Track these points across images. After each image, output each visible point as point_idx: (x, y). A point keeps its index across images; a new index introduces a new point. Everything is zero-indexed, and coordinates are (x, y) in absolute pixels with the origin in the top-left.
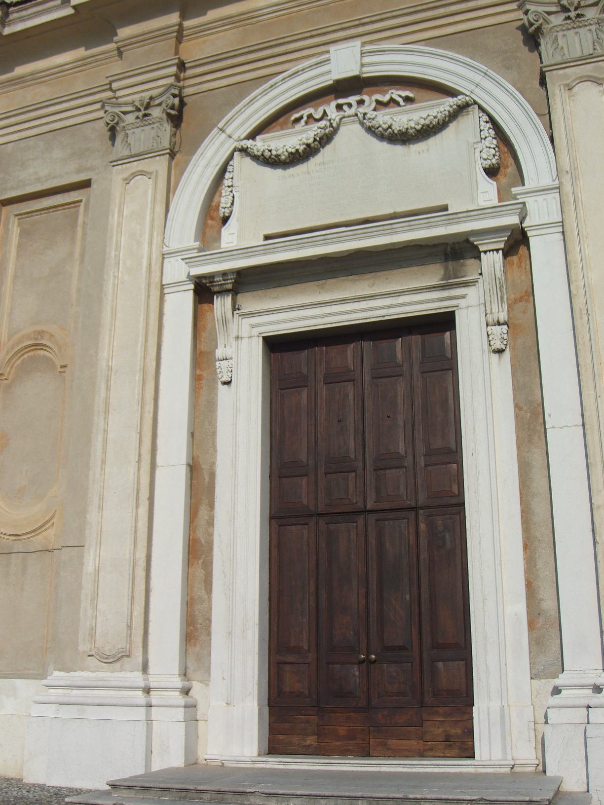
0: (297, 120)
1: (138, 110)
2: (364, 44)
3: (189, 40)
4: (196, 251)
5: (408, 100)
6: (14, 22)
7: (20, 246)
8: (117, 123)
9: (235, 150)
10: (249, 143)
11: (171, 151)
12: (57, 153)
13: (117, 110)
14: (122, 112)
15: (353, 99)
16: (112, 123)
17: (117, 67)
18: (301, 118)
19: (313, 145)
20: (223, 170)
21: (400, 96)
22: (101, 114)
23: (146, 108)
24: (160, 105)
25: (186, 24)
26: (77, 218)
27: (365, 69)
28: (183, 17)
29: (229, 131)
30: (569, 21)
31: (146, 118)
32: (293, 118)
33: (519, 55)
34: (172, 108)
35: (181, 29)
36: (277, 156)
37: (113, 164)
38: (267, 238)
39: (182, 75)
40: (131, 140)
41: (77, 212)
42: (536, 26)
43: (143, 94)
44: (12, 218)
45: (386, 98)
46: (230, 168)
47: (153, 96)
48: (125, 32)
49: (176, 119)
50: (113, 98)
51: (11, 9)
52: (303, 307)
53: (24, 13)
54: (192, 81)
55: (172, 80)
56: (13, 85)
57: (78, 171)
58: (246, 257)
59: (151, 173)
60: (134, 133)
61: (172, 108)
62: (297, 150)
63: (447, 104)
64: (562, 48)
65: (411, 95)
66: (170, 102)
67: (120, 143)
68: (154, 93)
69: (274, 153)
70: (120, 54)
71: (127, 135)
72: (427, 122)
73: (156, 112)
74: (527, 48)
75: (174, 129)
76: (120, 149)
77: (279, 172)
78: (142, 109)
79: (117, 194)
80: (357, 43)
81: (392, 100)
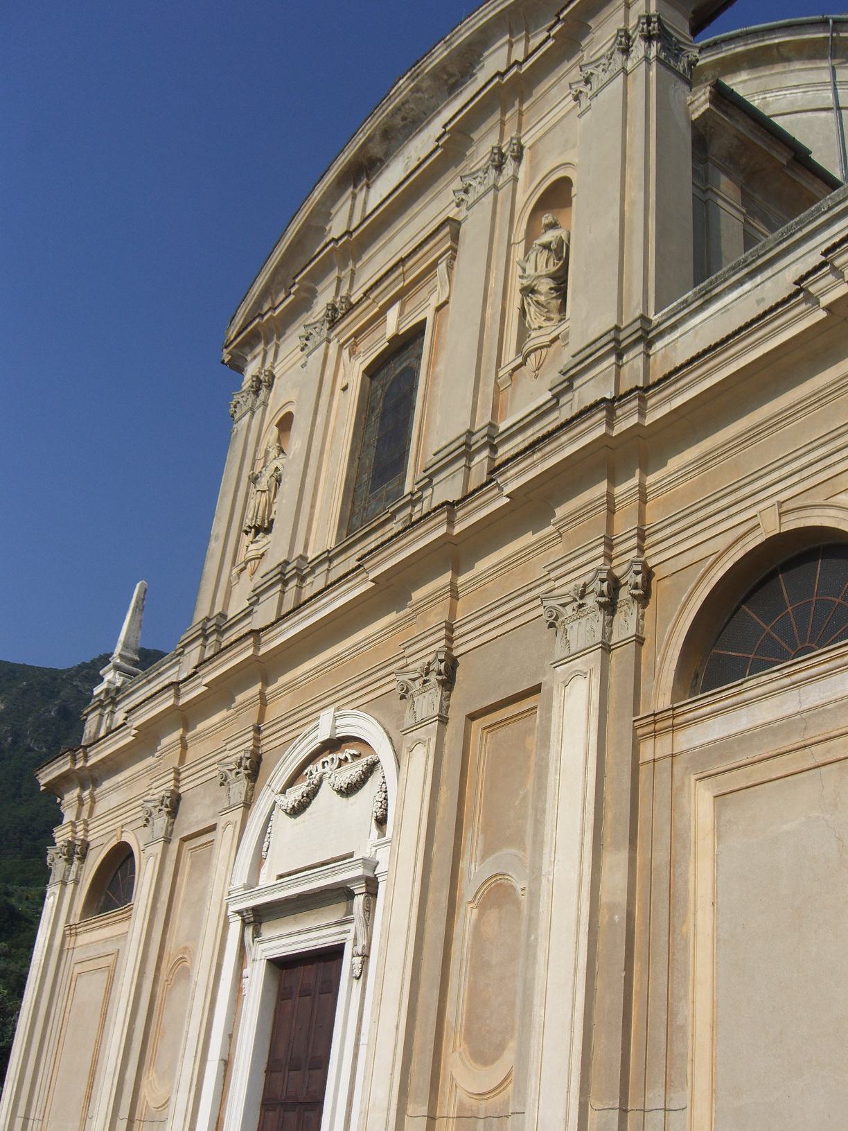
1: (575, 600)
2: (338, 709)
4: (243, 889)
6: (267, 643)
7: (190, 875)
19: (302, 800)
20: (269, 819)
22: (541, 611)
23: (581, 598)
24: (592, 591)
27: (338, 731)
37: (404, 733)
38: (280, 877)
43: (577, 582)
47: (587, 582)
52: (282, 937)
54: (186, 781)
56: (195, 739)
58: (252, 899)
62: (294, 806)
65: (356, 753)
68: (587, 579)
71: (566, 631)
73: (591, 601)
78: (578, 599)
80: (331, 709)
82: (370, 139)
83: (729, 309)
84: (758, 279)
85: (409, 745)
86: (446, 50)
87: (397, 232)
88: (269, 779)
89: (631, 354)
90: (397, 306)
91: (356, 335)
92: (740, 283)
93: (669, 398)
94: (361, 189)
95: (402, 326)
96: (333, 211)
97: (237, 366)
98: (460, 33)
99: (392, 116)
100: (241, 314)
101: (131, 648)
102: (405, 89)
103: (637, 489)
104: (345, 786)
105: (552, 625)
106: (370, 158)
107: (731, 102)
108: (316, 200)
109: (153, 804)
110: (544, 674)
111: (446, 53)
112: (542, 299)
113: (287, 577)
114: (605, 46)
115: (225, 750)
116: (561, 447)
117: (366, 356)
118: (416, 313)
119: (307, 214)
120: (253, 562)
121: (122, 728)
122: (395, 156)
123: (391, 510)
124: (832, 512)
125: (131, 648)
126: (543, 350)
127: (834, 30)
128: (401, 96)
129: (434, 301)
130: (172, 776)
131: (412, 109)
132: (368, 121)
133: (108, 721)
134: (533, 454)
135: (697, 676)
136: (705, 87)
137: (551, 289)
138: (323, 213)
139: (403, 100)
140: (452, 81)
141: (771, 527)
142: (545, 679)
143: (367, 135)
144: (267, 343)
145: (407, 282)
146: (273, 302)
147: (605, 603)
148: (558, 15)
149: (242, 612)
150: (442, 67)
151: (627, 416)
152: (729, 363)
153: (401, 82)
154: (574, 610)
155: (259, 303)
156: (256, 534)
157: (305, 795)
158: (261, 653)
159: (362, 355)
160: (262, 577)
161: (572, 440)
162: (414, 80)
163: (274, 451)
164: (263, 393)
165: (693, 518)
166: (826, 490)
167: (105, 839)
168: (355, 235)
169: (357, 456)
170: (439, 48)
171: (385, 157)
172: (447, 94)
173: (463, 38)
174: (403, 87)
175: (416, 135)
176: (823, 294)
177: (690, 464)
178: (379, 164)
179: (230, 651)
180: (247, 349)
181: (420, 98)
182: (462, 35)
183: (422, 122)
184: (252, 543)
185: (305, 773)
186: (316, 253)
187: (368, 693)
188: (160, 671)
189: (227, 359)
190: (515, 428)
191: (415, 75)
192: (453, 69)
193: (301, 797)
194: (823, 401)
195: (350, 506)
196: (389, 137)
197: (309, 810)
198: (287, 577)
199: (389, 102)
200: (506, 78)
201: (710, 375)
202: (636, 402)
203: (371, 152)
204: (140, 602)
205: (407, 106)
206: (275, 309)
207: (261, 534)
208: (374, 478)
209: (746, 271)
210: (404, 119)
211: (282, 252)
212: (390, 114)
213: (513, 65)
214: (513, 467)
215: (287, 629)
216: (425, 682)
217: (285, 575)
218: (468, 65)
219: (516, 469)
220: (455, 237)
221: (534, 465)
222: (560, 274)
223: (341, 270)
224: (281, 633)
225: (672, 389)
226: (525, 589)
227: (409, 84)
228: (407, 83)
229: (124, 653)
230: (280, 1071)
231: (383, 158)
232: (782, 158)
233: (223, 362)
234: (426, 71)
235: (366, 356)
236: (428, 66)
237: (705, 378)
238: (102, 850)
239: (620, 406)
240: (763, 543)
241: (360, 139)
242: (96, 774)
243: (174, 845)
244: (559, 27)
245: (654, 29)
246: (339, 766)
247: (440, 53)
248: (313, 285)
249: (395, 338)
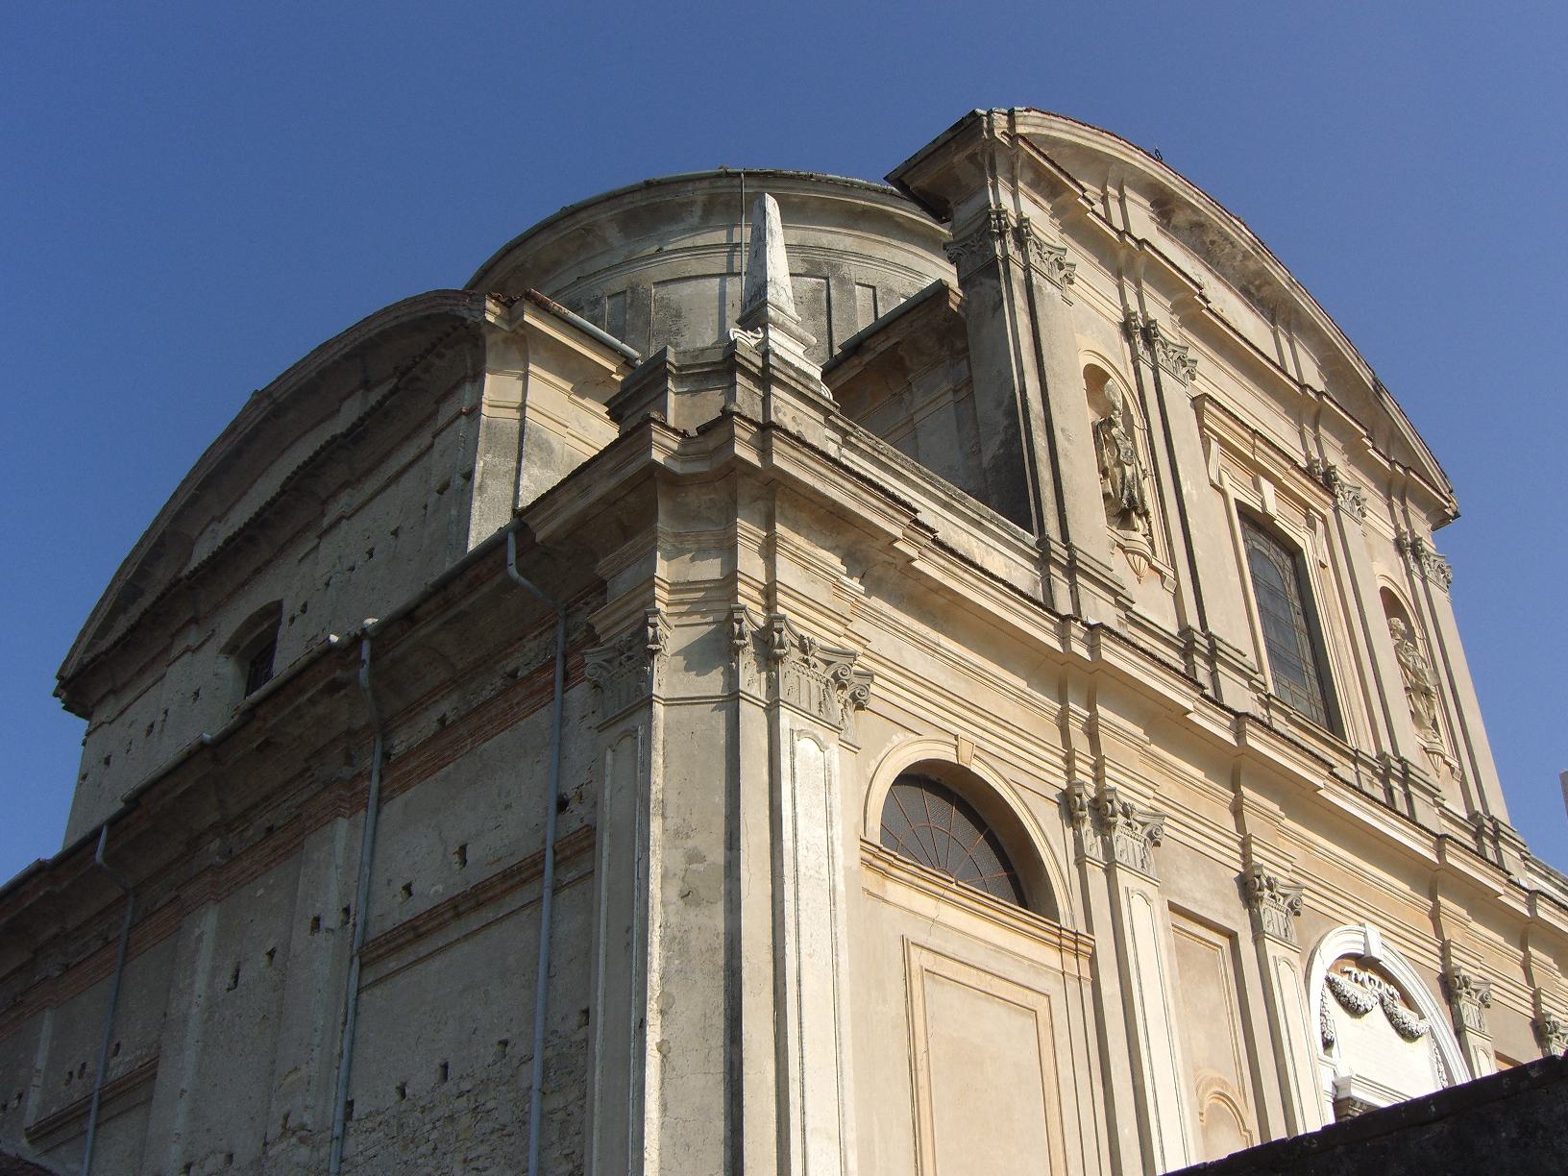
58: (1379, 1097)
106: (1174, 211)
118: (1241, 489)
122: (1182, 247)
140: (1253, 290)
148: (1410, 468)
150: (1269, 280)
162: (1253, 249)
179: (1297, 752)
181: (1235, 258)
186: (1081, 183)
192: (1266, 291)
203: (1181, 212)
210: (1213, 243)
215: (1351, 802)
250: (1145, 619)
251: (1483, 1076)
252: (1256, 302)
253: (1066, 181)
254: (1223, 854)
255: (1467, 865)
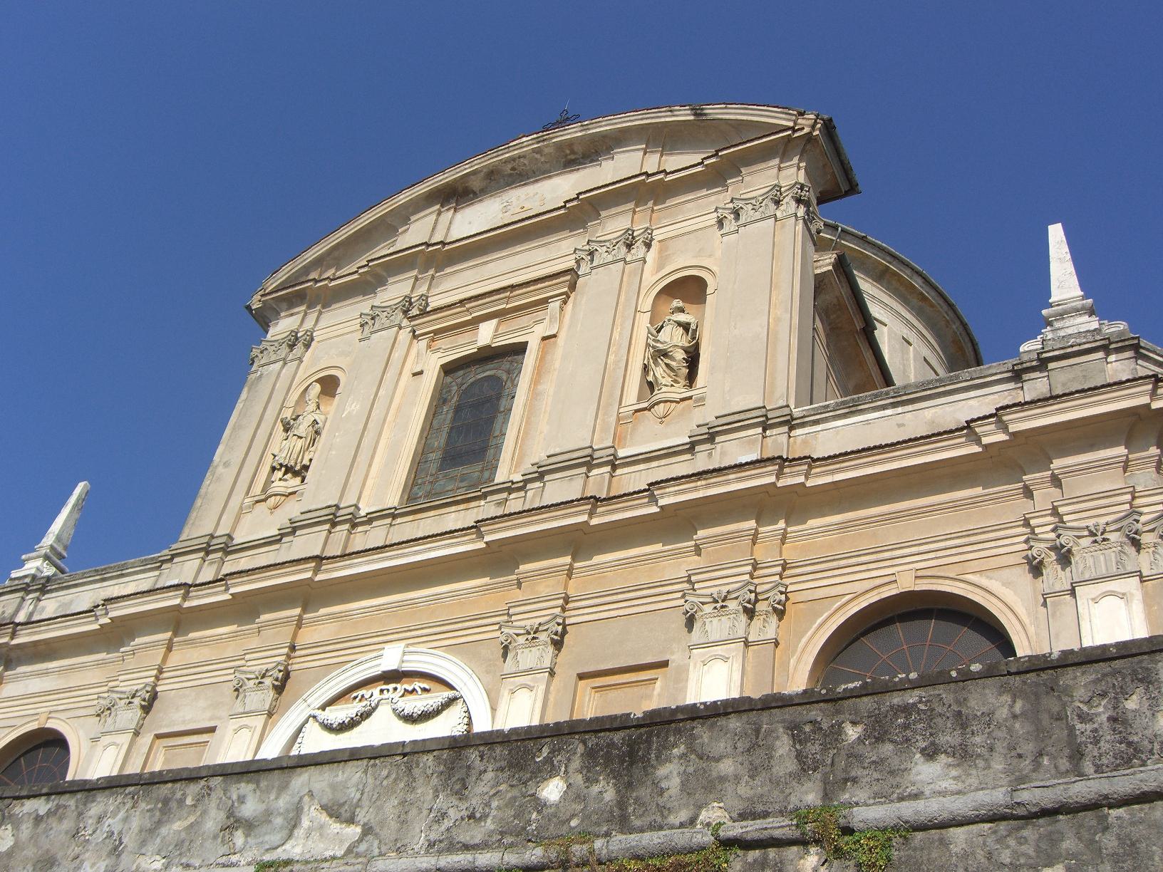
0: (355, 698)
1: (528, 633)
2: (408, 645)
3: (307, 627)
5: (425, 690)
8: (510, 643)
9: (310, 716)
10: (318, 713)
11: (269, 712)
12: (202, 703)
13: (243, 676)
14: (515, 634)
15: (391, 686)
16: (506, 643)
17: (518, 595)
18: (357, 697)
19: (355, 719)
20: (299, 730)
21: (420, 687)
25: (761, 529)
26: (204, 753)
27: (404, 665)
28: (574, 559)
29: (309, 702)
30: (527, 642)
31: (260, 685)
32: (352, 696)
33: (498, 663)
34: (556, 634)
35: (300, 619)
36: (331, 724)
39: (293, 655)
40: (118, 719)
41: (205, 750)
42: (1038, 560)
44: (161, 748)
45: (410, 688)
46: (304, 730)
48: (264, 617)
49: (280, 689)
50: (509, 622)
51: (19, 627)
53: (200, 593)
55: (747, 577)
57: (211, 719)
59: (251, 727)
60: (250, 695)
61: (556, 634)
62: (344, 722)
63: (444, 695)
64: (1061, 579)
65: (427, 687)
66: (554, 629)
67: (698, 629)
69: (329, 722)
70: (519, 585)
71: (245, 696)
72: (426, 709)
73: (137, 701)
74: (1031, 575)
75: (276, 696)
76: (509, 666)
77: (333, 736)
79: (227, 739)
80: (403, 644)
81: (414, 690)
82: (474, 173)
83: (870, 423)
84: (900, 410)
85: (512, 688)
86: (581, 131)
87: (492, 261)
88: (308, 693)
89: (775, 431)
90: (495, 321)
91: (436, 332)
92: (884, 407)
93: (833, 472)
94: (448, 210)
95: (497, 340)
96: (413, 218)
97: (263, 319)
98: (600, 124)
99: (505, 163)
100: (286, 271)
101: (63, 543)
102: (526, 146)
103: (782, 531)
104: (420, 713)
105: (237, 690)
106: (466, 187)
107: (844, 271)
108: (401, 203)
109: (119, 695)
110: (672, 653)
111: (580, 134)
112: (673, 364)
113: (338, 519)
114: (761, 190)
115: (118, 680)
116: (728, 482)
117: (445, 354)
119: (386, 211)
120: (278, 497)
121: (81, 615)
122: (491, 196)
123: (483, 490)
124: (962, 585)
125: (63, 543)
126: (672, 404)
127: (839, 237)
128: (522, 150)
129: (541, 330)
130: (155, 672)
131: (525, 164)
132: (478, 157)
133: (31, 607)
134: (697, 481)
135: (818, 681)
136: (833, 254)
137: (684, 359)
138: (404, 216)
139: (522, 154)
140: (572, 157)
141: (907, 584)
142: (673, 657)
143: (474, 168)
144: (309, 307)
145: (509, 306)
146: (320, 275)
147: (277, 686)
149: (263, 539)
150: (570, 144)
151: (793, 475)
152: (892, 461)
153: (525, 139)
154: (255, 684)
155: (307, 270)
156: (285, 473)
157: (359, 714)
158: (317, 579)
159: (441, 351)
160: (302, 513)
161: (740, 480)
162: (538, 142)
163: (313, 405)
164: (299, 348)
165: (835, 564)
166: (958, 569)
167: (18, 722)
168: (447, 248)
169: (425, 435)
170: (574, 128)
171: (480, 193)
172: (562, 165)
173: (602, 129)
174: (525, 144)
175: (519, 186)
176: (985, 436)
177: (832, 525)
178: (471, 196)
180: (284, 305)
181: (536, 159)
182: (601, 126)
183: (528, 178)
184: (280, 480)
185: (355, 694)
187: (449, 638)
188: (124, 572)
189: (256, 306)
190: (640, 457)
191: (541, 139)
192: (579, 149)
193: (354, 715)
194: (957, 508)
195: (413, 476)
196: (492, 178)
197: (356, 730)
198: (338, 519)
199: (506, 150)
200: (651, 180)
201: (874, 465)
202: (806, 467)
204: (80, 502)
205: (522, 160)
206: (332, 280)
207: (289, 475)
208: (444, 459)
209: (891, 400)
210: (513, 169)
211: (349, 233)
212: (503, 161)
213: (661, 172)
214: (674, 486)
215: (360, 564)
216: (130, 703)
217: (336, 517)
218: (593, 151)
219: (677, 488)
220: (573, 287)
221: (696, 489)
222: (692, 350)
223: (420, 272)
224: (350, 566)
225: (838, 466)
226: (659, 584)
227: (533, 144)
228: (530, 142)
229: (55, 545)
230: (1062, 719)
231: (478, 192)
232: (859, 325)
233: (249, 308)
234: (553, 141)
235: (445, 354)
236: (556, 137)
237: (871, 466)
238: (9, 733)
239: (789, 466)
240: (897, 595)
241: (465, 169)
242: (13, 655)
243: (145, 739)
244: (713, 160)
245: (805, 196)
246: (403, 696)
247: (573, 132)
248: (385, 274)
249: (487, 348)
250: (652, 452)
251: (1087, 643)
252: (581, 160)
253: (301, 287)
254: (928, 560)
255: (270, 579)
